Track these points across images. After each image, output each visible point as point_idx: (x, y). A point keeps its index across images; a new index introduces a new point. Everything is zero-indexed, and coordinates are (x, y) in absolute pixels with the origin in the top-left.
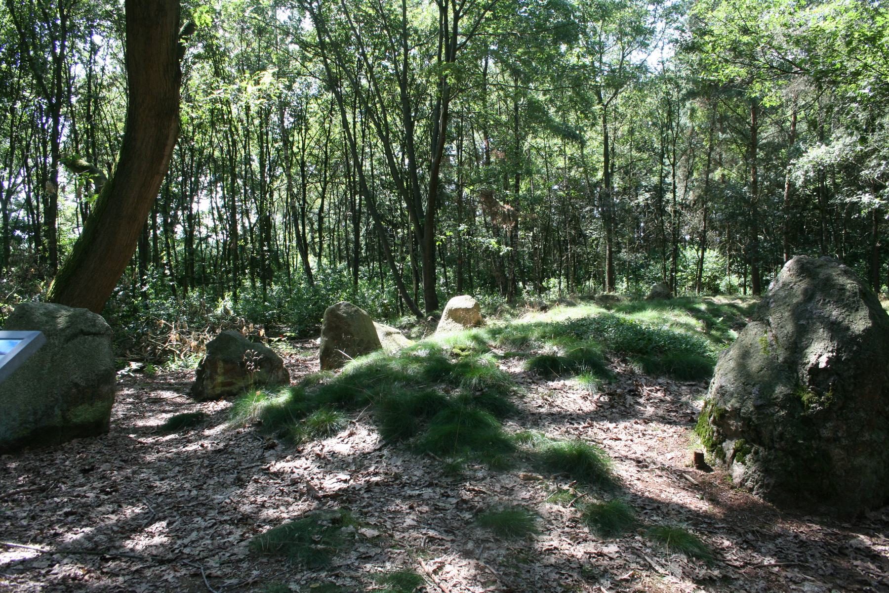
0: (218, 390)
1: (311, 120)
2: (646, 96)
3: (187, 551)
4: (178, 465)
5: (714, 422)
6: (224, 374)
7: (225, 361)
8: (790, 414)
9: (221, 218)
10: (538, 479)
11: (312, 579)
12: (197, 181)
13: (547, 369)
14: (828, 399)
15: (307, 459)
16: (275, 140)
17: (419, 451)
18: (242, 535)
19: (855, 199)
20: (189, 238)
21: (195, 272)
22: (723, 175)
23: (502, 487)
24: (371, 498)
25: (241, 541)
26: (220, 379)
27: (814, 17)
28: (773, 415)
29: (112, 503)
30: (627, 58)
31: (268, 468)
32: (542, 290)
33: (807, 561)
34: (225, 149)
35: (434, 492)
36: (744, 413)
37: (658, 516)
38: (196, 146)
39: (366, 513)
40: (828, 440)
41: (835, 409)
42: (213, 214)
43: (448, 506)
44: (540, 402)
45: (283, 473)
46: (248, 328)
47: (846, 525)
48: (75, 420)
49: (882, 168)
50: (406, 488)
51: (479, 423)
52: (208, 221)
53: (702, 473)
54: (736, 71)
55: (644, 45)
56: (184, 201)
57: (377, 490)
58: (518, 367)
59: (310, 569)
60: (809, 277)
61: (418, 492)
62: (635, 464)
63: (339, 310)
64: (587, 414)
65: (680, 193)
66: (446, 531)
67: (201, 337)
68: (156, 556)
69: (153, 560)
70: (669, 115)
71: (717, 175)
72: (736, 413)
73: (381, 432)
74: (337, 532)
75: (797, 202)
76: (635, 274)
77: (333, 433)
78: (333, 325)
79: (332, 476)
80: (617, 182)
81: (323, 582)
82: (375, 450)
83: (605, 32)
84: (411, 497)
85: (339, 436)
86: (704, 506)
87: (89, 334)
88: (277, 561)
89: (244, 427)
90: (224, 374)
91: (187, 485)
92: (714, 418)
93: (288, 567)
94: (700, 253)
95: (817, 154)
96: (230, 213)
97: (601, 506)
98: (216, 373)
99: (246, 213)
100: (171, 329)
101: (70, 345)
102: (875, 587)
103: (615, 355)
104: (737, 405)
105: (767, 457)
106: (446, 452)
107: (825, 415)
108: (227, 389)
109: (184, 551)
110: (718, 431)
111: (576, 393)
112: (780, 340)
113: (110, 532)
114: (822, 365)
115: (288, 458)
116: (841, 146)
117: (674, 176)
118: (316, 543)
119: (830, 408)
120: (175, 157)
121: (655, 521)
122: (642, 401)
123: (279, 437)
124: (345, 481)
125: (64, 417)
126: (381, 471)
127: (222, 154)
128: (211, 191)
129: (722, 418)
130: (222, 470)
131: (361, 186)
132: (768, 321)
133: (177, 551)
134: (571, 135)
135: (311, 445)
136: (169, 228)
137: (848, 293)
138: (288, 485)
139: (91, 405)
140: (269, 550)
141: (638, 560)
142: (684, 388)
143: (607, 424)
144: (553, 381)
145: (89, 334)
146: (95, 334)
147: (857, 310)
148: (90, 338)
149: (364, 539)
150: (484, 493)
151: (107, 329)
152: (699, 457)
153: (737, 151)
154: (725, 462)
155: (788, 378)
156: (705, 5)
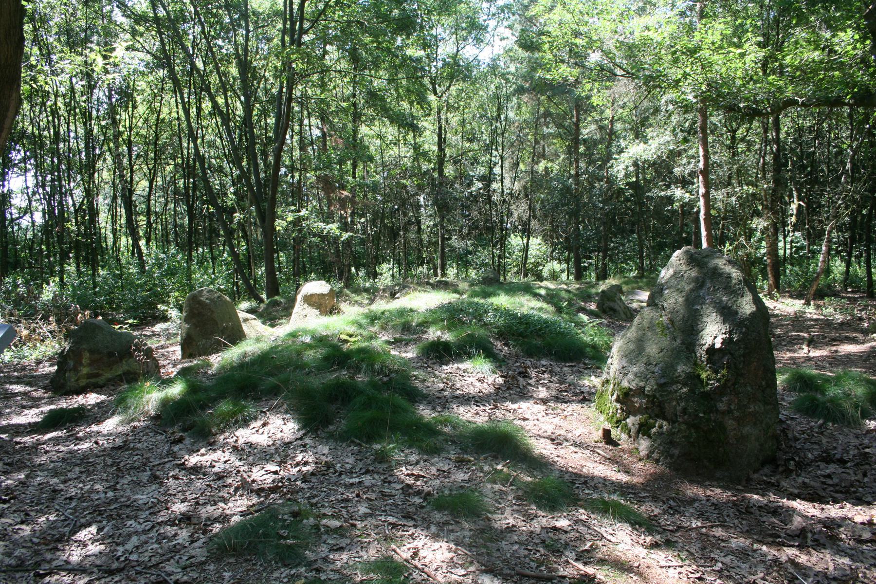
0: (83, 382)
1: (139, 99)
2: (478, 89)
3: (134, 557)
4: (77, 465)
5: (617, 400)
6: (90, 365)
7: (91, 352)
8: (692, 391)
10: (470, 461)
11: (292, 576)
13: (440, 353)
14: (723, 376)
15: (224, 452)
17: (343, 438)
18: (191, 536)
19: (669, 193)
22: (546, 168)
23: (438, 470)
24: (312, 488)
25: (192, 542)
27: (637, 28)
28: (676, 391)
29: (15, 511)
30: (461, 52)
31: (184, 463)
32: (375, 275)
33: (725, 521)
35: (374, 479)
36: (649, 391)
37: (588, 489)
39: (316, 504)
40: (723, 413)
41: (729, 384)
43: (394, 492)
44: (441, 386)
45: (201, 467)
47: (740, 487)
49: (692, 166)
50: (343, 476)
51: (396, 409)
53: (611, 447)
54: (566, 72)
55: (478, 40)
57: (314, 480)
58: (410, 353)
59: (285, 566)
61: (357, 480)
62: (549, 442)
64: (489, 395)
65: (507, 182)
66: (404, 517)
67: (32, 326)
68: (101, 566)
69: (100, 571)
70: (499, 109)
71: (541, 167)
72: (640, 391)
73: (299, 421)
74: (300, 526)
75: (613, 193)
76: (463, 261)
77: (246, 423)
78: (195, 311)
79: (258, 467)
80: (449, 170)
81: (306, 577)
82: (297, 439)
83: (442, 29)
84: (352, 485)
85: (252, 426)
86: (623, 478)
88: (246, 561)
89: (139, 421)
90: (90, 365)
91: (98, 487)
92: (618, 396)
93: (261, 565)
94: (525, 240)
97: (536, 484)
98: (81, 364)
102: (785, 538)
103: (498, 339)
104: (642, 384)
106: (371, 438)
107: (720, 391)
108: (93, 380)
109: (131, 558)
110: (621, 408)
111: (476, 374)
112: (677, 324)
113: (29, 544)
114: (718, 346)
115: (203, 451)
116: (657, 145)
117: (502, 167)
118: (285, 538)
119: (725, 384)
121: (588, 494)
122: (532, 382)
123: (184, 430)
124: (276, 473)
126: (310, 460)
129: (625, 397)
130: (131, 468)
131: (194, 169)
132: (663, 306)
133: (122, 559)
134: (408, 124)
135: (222, 437)
137: (734, 281)
138: (214, 480)
140: (234, 550)
141: (589, 531)
142: (566, 369)
143: (510, 406)
144: (447, 365)
147: (742, 296)
149: (329, 531)
150: (424, 477)
152: (607, 433)
153: (558, 146)
154: (630, 437)
155: (687, 358)
156: (543, 8)
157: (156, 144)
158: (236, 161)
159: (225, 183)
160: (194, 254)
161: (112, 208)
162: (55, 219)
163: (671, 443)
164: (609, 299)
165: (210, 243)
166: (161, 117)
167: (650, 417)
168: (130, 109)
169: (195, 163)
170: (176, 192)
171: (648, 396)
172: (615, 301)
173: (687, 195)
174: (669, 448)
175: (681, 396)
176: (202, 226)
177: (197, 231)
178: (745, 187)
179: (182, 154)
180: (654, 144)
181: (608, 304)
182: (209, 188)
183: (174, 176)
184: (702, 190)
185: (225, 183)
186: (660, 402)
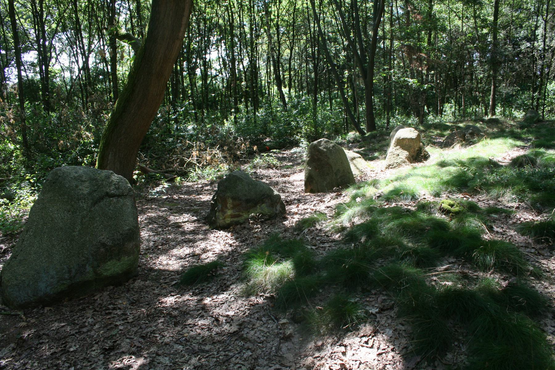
0: (228, 221)
6: (233, 208)
7: (234, 199)
9: (225, 64)
12: (209, 40)
16: (259, 11)
20: (205, 76)
21: (209, 102)
26: (229, 212)
34: (226, 18)
38: (208, 17)
42: (219, 61)
46: (245, 144)
48: (105, 274)
52: (216, 65)
56: (201, 52)
63: (320, 146)
67: (214, 152)
87: (113, 196)
96: (230, 62)
98: (226, 207)
99: (241, 61)
100: (193, 147)
101: (97, 207)
108: (235, 219)
120: (194, 24)
125: (95, 272)
127: (224, 21)
128: (217, 46)
131: (319, 41)
136: (192, 71)
139: (119, 260)
145: (113, 196)
146: (119, 196)
148: (115, 200)
151: (130, 190)
157: (293, 26)
158: (345, 33)
159: (339, 49)
160: (318, 96)
161: (268, 66)
162: (234, 78)
165: (329, 88)
166: (297, 7)
168: (278, 4)
169: (319, 37)
170: (307, 56)
176: (321, 79)
177: (320, 80)
179: (310, 32)
182: (328, 53)
183: (306, 46)
185: (339, 49)
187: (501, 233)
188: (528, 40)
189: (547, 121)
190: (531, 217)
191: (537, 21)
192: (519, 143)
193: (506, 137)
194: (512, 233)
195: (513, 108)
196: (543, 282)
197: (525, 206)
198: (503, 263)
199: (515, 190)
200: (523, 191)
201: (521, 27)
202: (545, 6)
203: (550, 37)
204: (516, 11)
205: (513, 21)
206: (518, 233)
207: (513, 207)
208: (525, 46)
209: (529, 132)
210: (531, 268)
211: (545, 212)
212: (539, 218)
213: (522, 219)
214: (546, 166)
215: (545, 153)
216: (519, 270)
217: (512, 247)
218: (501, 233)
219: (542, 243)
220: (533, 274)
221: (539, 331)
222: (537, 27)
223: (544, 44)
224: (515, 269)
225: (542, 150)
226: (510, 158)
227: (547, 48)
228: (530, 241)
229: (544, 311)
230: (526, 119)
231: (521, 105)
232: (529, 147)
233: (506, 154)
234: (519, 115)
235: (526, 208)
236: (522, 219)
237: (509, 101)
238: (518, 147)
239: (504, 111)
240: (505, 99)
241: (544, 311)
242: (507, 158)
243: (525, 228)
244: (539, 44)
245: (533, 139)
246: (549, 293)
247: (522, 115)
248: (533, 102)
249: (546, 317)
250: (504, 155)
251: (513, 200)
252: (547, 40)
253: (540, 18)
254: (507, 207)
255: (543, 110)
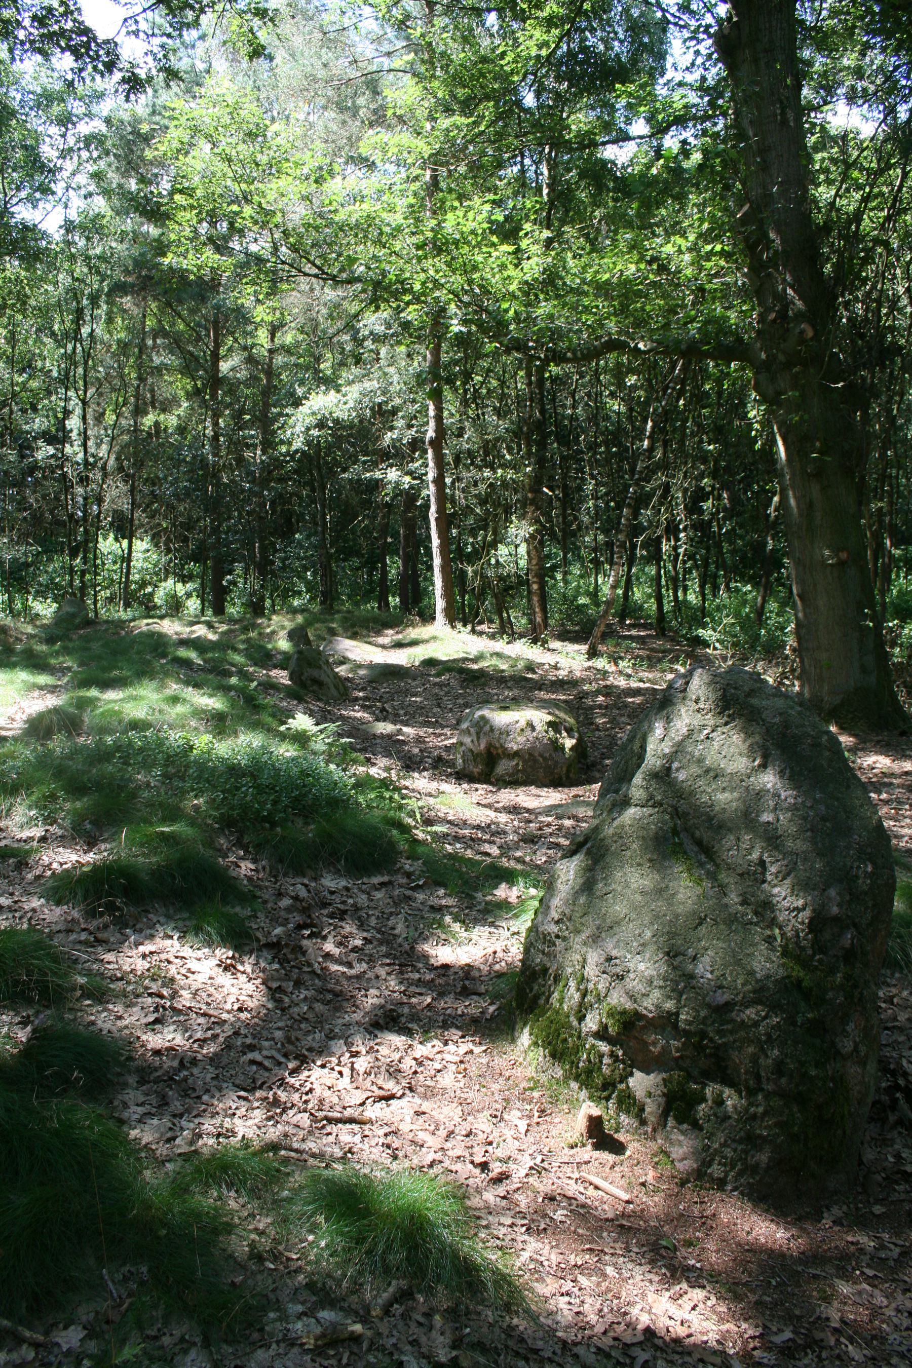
19: (378, 475)
60: (741, 715)
71: (149, 420)
72: (666, 1022)
94: (125, 543)
95: (322, 402)
104: (669, 1005)
105: (747, 1110)
110: (612, 1055)
116: (356, 395)
153: (176, 385)
154: (643, 1122)
163: (751, 1141)
164: (310, 665)
167: (689, 1077)
171: (686, 1033)
172: (320, 667)
173: (407, 479)
174: (746, 1152)
175: (768, 1035)
178: (500, 472)
180: (353, 393)
181: (309, 672)
184: (431, 475)
186: (718, 1048)
187: (10, 909)
188: (51, 439)
189: (107, 622)
190: (74, 857)
191: (67, 400)
192: (43, 679)
193: (11, 666)
194: (36, 903)
195: (28, 593)
196: (111, 1007)
197: (60, 832)
198: (17, 982)
199: (33, 798)
200: (53, 797)
201: (35, 409)
202: (80, 370)
203: (97, 438)
204: (22, 371)
205: (15, 395)
206: (48, 900)
207: (32, 839)
208: (44, 451)
209: (66, 651)
210: (82, 980)
211: (104, 841)
212: (90, 857)
213: (55, 865)
214: (103, 730)
215: (98, 699)
216: (55, 991)
217: (36, 937)
218: (9, 907)
219: (102, 914)
220: (87, 993)
221: (111, 1124)
222: (67, 413)
223: (86, 452)
224: (44, 989)
225: (93, 692)
226: (25, 717)
227: (91, 460)
228: (75, 914)
229: (120, 1075)
230: (60, 619)
231: (47, 586)
232: (65, 687)
233: (16, 707)
234: (46, 609)
235: (62, 837)
236: (55, 865)
237: (22, 578)
238: (41, 688)
239: (11, 600)
240: (11, 573)
241: (120, 1075)
242: (18, 717)
243: (63, 888)
244: (74, 450)
245: (75, 668)
246: (126, 1027)
247: (52, 610)
248: (72, 581)
249: (126, 1085)
250: (11, 711)
251: (30, 822)
252: (90, 443)
253: (71, 393)
254: (19, 841)
255: (95, 596)
